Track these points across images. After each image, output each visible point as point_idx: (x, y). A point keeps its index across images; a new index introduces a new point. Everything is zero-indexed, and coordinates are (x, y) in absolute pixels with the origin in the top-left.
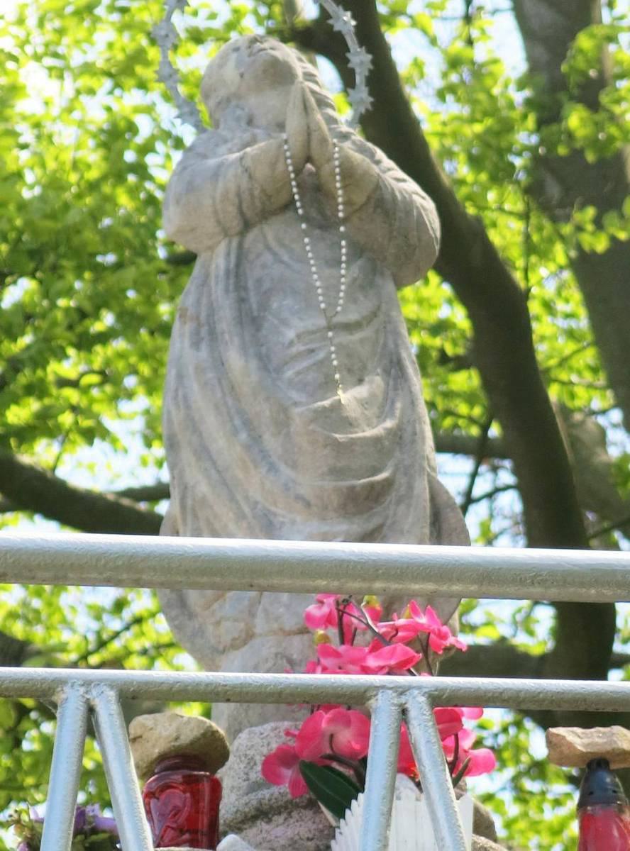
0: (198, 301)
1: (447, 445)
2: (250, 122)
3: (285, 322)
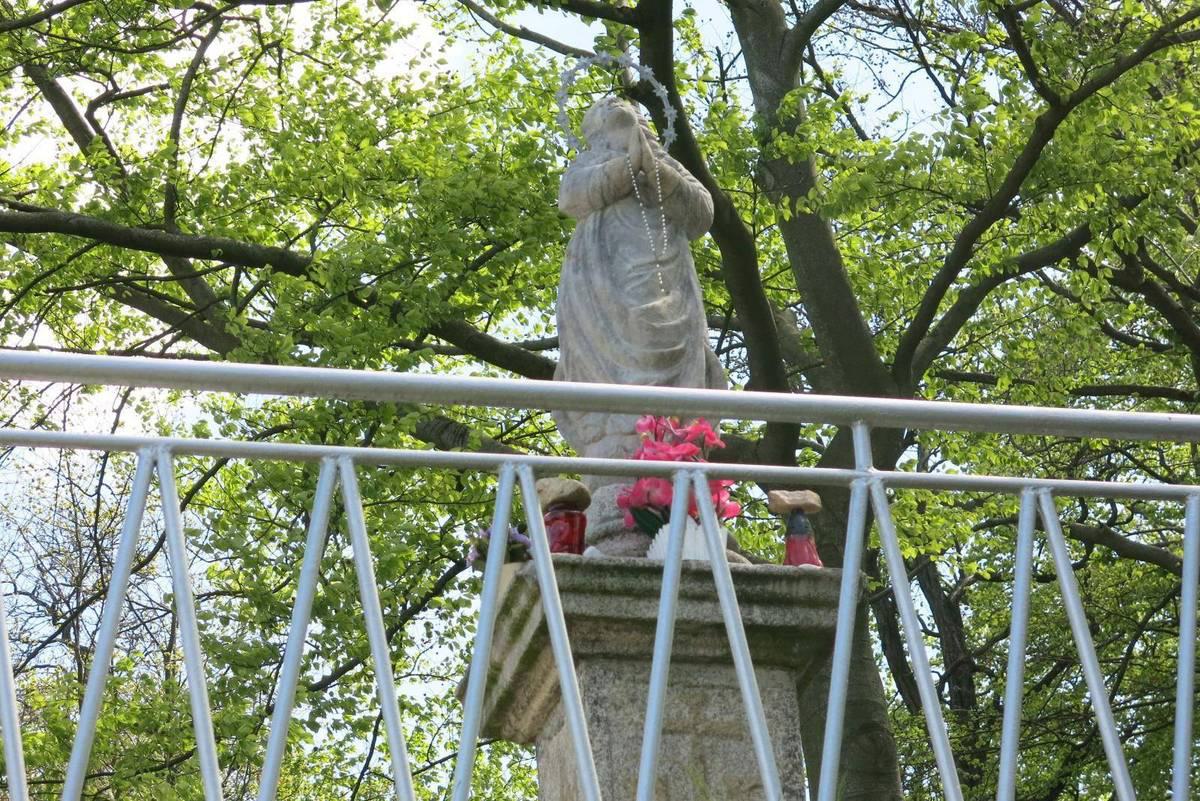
0: (577, 248)
1: (712, 325)
2: (608, 147)
3: (626, 260)
